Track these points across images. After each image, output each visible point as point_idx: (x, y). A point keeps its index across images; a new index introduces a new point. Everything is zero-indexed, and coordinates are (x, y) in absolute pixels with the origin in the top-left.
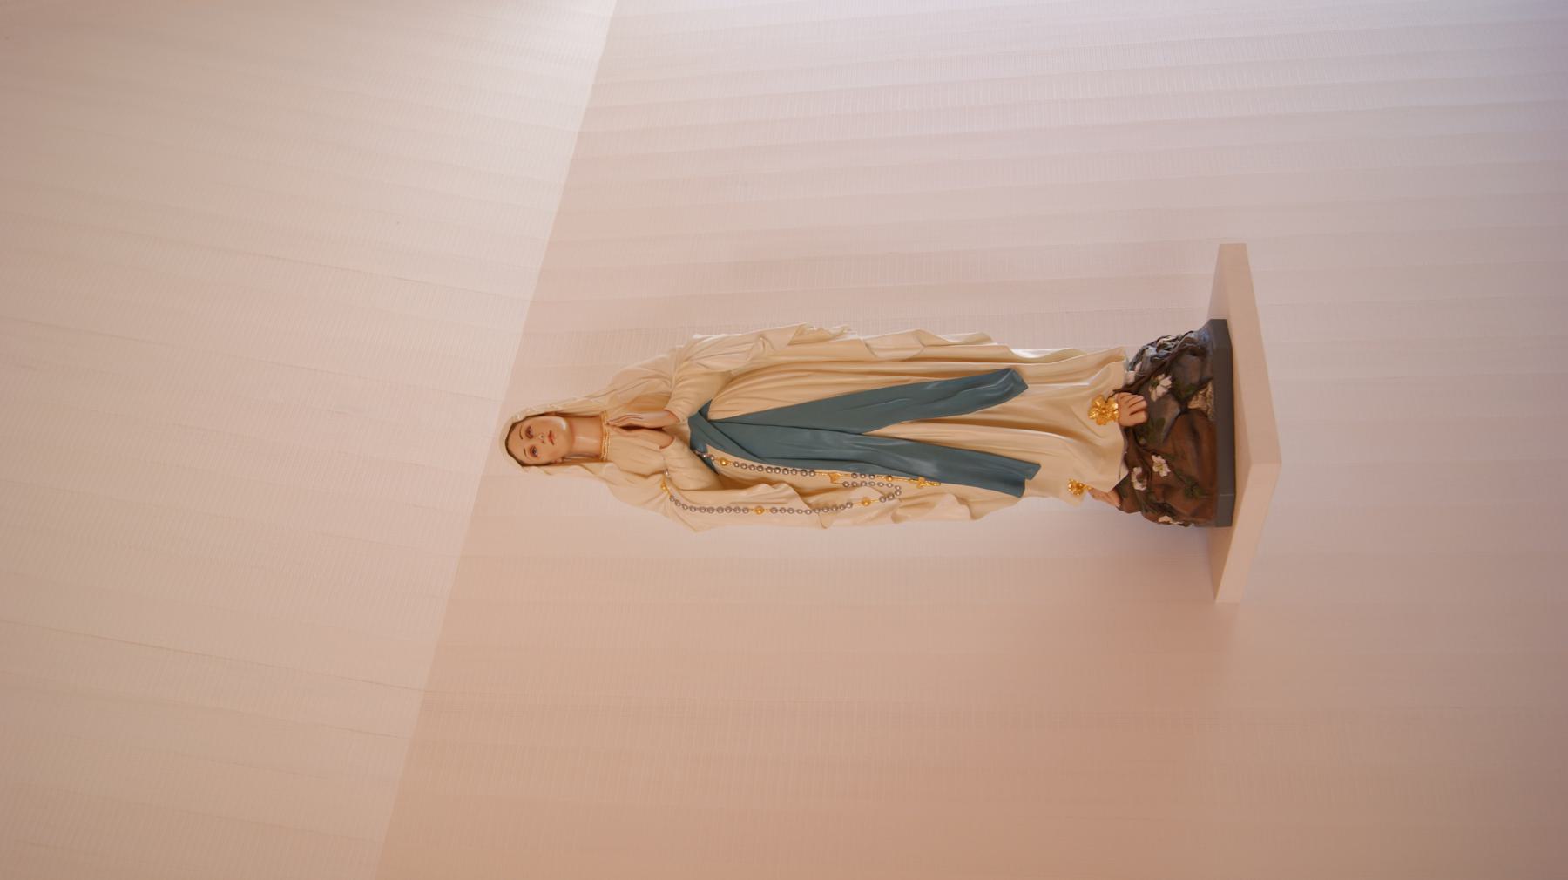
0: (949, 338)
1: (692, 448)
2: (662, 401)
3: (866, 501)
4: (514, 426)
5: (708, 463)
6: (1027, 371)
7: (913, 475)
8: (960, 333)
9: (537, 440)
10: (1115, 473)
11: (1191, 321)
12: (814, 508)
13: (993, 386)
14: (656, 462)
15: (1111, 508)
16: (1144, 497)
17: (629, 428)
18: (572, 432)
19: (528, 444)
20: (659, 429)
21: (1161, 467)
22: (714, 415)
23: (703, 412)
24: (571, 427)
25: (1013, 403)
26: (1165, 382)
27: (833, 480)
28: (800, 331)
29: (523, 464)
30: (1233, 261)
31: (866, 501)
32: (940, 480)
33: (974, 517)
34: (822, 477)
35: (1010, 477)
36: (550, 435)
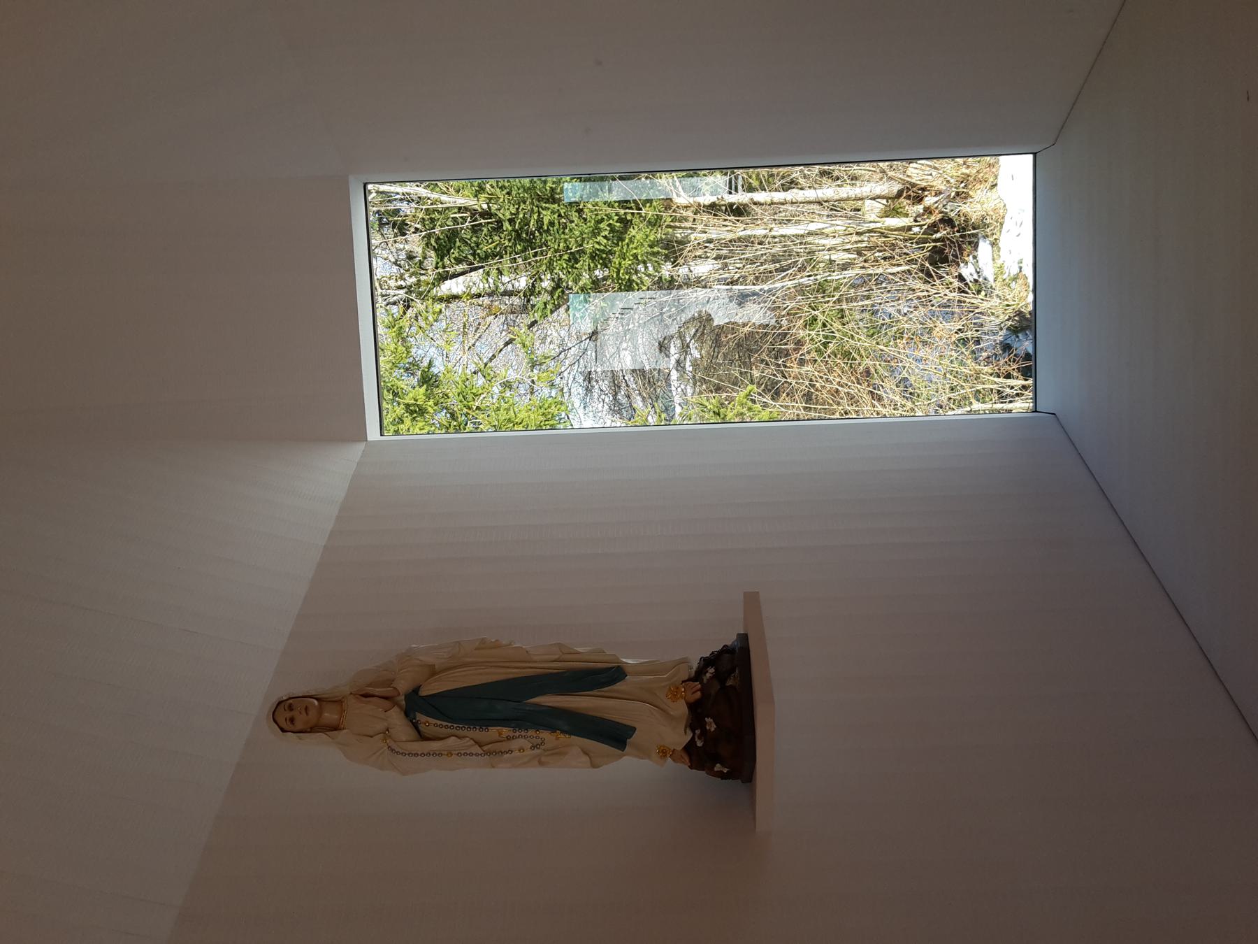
0: (579, 650)
1: (407, 714)
2: (389, 683)
3: (521, 749)
4: (279, 703)
5: (415, 726)
6: (627, 670)
7: (553, 729)
8: (586, 648)
9: (297, 715)
10: (679, 737)
11: (730, 639)
12: (486, 753)
13: (605, 676)
14: (380, 726)
15: (679, 770)
16: (699, 756)
17: (366, 696)
18: (320, 711)
19: (289, 715)
20: (386, 698)
21: (711, 726)
22: (424, 692)
23: (416, 691)
24: (320, 705)
25: (619, 686)
26: (712, 670)
27: (500, 734)
28: (483, 641)
29: (283, 730)
30: (752, 601)
31: (521, 749)
32: (571, 734)
33: (594, 766)
34: (493, 732)
35: (616, 736)
36: (306, 709)
